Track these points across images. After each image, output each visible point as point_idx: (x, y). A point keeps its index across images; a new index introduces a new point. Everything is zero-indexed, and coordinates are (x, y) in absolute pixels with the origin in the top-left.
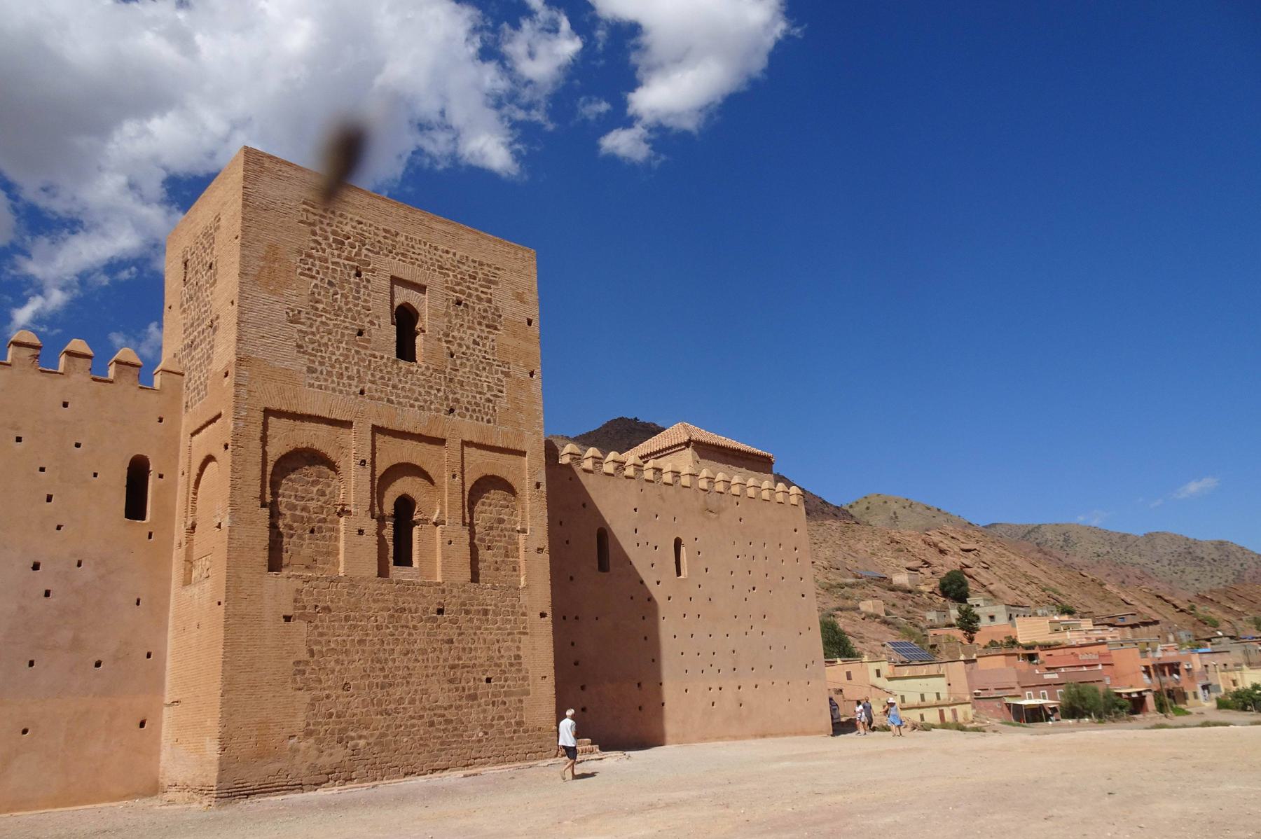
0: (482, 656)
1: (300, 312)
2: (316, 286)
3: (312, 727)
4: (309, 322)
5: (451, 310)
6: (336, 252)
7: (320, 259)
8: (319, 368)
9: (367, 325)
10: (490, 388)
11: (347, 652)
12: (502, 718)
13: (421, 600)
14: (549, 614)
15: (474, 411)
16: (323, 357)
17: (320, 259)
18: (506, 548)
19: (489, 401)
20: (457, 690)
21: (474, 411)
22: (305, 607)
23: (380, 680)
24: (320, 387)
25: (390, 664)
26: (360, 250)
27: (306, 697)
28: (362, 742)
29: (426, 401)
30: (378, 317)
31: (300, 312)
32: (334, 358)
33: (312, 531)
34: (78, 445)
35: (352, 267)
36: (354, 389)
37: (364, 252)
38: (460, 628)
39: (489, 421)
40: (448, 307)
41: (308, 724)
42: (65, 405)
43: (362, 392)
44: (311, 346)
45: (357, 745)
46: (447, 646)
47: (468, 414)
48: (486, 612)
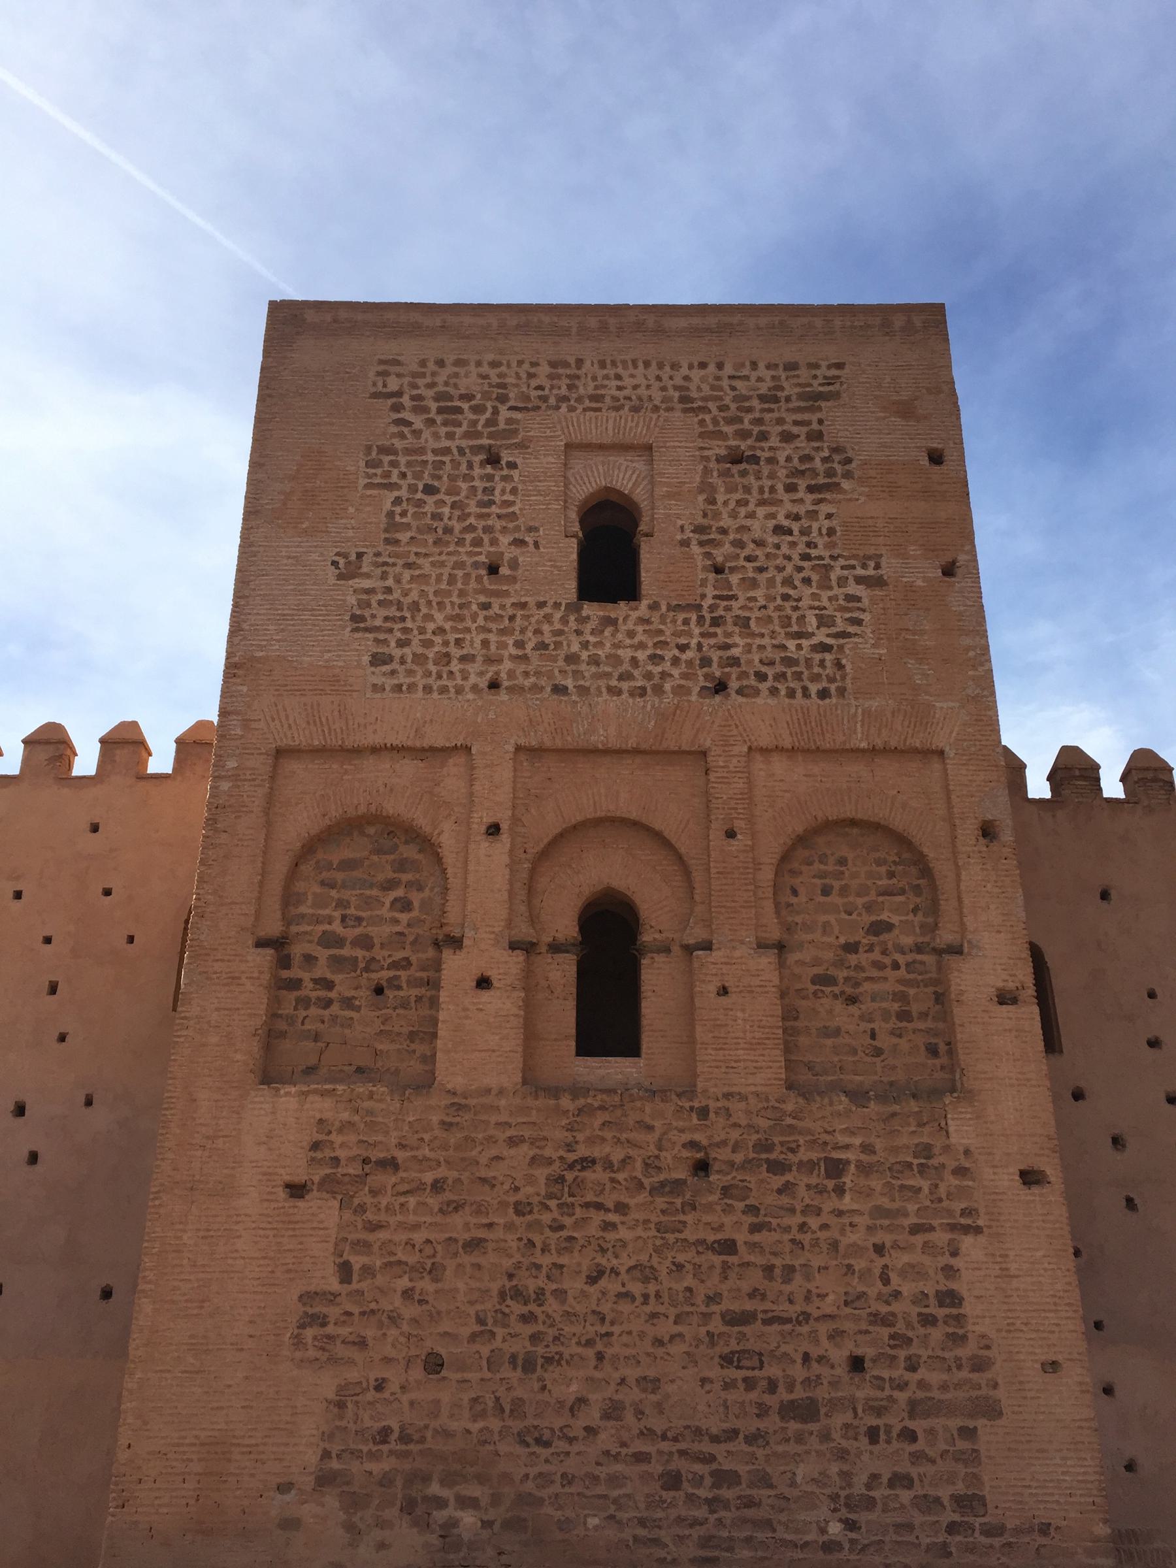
0: (832, 1290)
1: (360, 555)
2: (397, 501)
3: (335, 1465)
4: (379, 571)
5: (714, 479)
6: (443, 430)
7: (408, 451)
8: (397, 653)
9: (509, 553)
10: (823, 621)
11: (435, 1272)
12: (905, 1481)
13: (638, 1136)
14: (1053, 1172)
15: (781, 677)
16: (406, 630)
17: (408, 451)
18: (902, 997)
19: (826, 648)
20: (750, 1384)
21: (781, 677)
22: (336, 1161)
23: (520, 1347)
24: (398, 688)
25: (552, 1306)
26: (496, 411)
27: (327, 1384)
28: (468, 1519)
29: (648, 676)
30: (531, 529)
31: (360, 555)
32: (431, 626)
33: (379, 991)
34: (107, 892)
35: (476, 450)
36: (473, 679)
37: (504, 413)
38: (752, 1210)
39: (824, 694)
40: (707, 471)
41: (326, 1455)
42: (95, 828)
43: (494, 685)
44: (383, 612)
45: (453, 1523)
46: (717, 1260)
47: (764, 687)
48: (836, 1168)
